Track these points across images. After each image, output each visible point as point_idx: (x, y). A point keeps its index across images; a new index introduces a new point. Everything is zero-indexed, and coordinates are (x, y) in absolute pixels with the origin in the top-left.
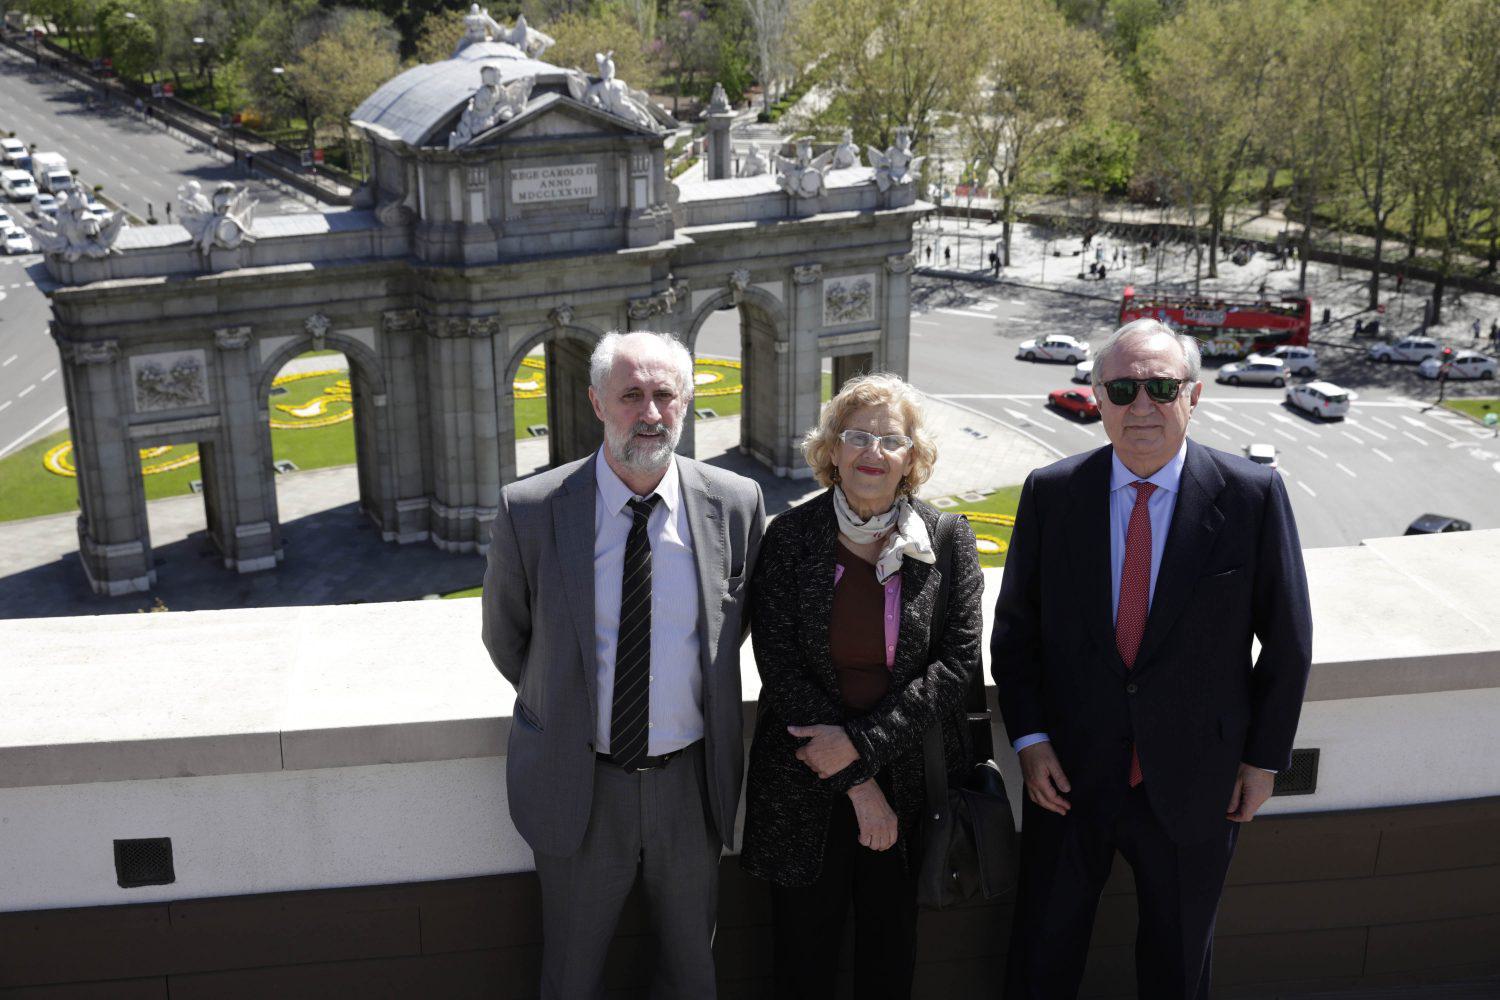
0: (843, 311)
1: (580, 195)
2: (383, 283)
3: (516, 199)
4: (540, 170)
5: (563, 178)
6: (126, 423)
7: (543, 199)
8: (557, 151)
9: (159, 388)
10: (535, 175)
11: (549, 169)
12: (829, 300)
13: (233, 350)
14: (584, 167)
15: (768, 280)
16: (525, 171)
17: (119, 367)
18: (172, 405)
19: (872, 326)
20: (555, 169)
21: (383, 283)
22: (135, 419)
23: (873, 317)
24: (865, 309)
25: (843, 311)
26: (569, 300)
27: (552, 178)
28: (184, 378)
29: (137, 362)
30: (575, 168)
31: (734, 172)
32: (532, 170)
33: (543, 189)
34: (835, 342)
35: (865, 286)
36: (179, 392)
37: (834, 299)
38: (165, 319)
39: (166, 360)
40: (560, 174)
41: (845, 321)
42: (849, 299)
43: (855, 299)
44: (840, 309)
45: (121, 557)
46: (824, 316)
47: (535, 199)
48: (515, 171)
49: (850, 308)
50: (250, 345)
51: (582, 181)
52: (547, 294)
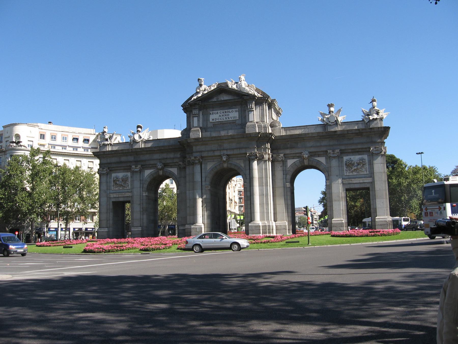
0: (353, 169)
1: (232, 119)
2: (179, 153)
3: (211, 120)
4: (219, 111)
5: (227, 114)
6: (108, 192)
7: (220, 120)
8: (224, 105)
9: (118, 183)
10: (217, 113)
11: (222, 111)
12: (346, 164)
13: (136, 172)
14: (234, 110)
15: (319, 156)
16: (214, 112)
17: (109, 176)
18: (121, 188)
19: (367, 176)
20: (224, 111)
21: (179, 153)
22: (111, 191)
23: (368, 173)
24: (364, 169)
25: (353, 169)
26: (225, 152)
27: (223, 114)
28: (125, 180)
29: (114, 175)
30: (231, 110)
31: (369, 180)
32: (216, 112)
33: (220, 117)
34: (351, 182)
35: (362, 159)
36: (123, 184)
37: (348, 164)
38: (121, 162)
39: (121, 175)
40: (225, 112)
41: (355, 173)
42: (356, 164)
43: (358, 164)
44: (352, 168)
45: (436, 335)
46: (345, 171)
47: (217, 121)
48: (211, 112)
49: (356, 168)
50: (141, 171)
51: (234, 114)
52: (218, 150)
